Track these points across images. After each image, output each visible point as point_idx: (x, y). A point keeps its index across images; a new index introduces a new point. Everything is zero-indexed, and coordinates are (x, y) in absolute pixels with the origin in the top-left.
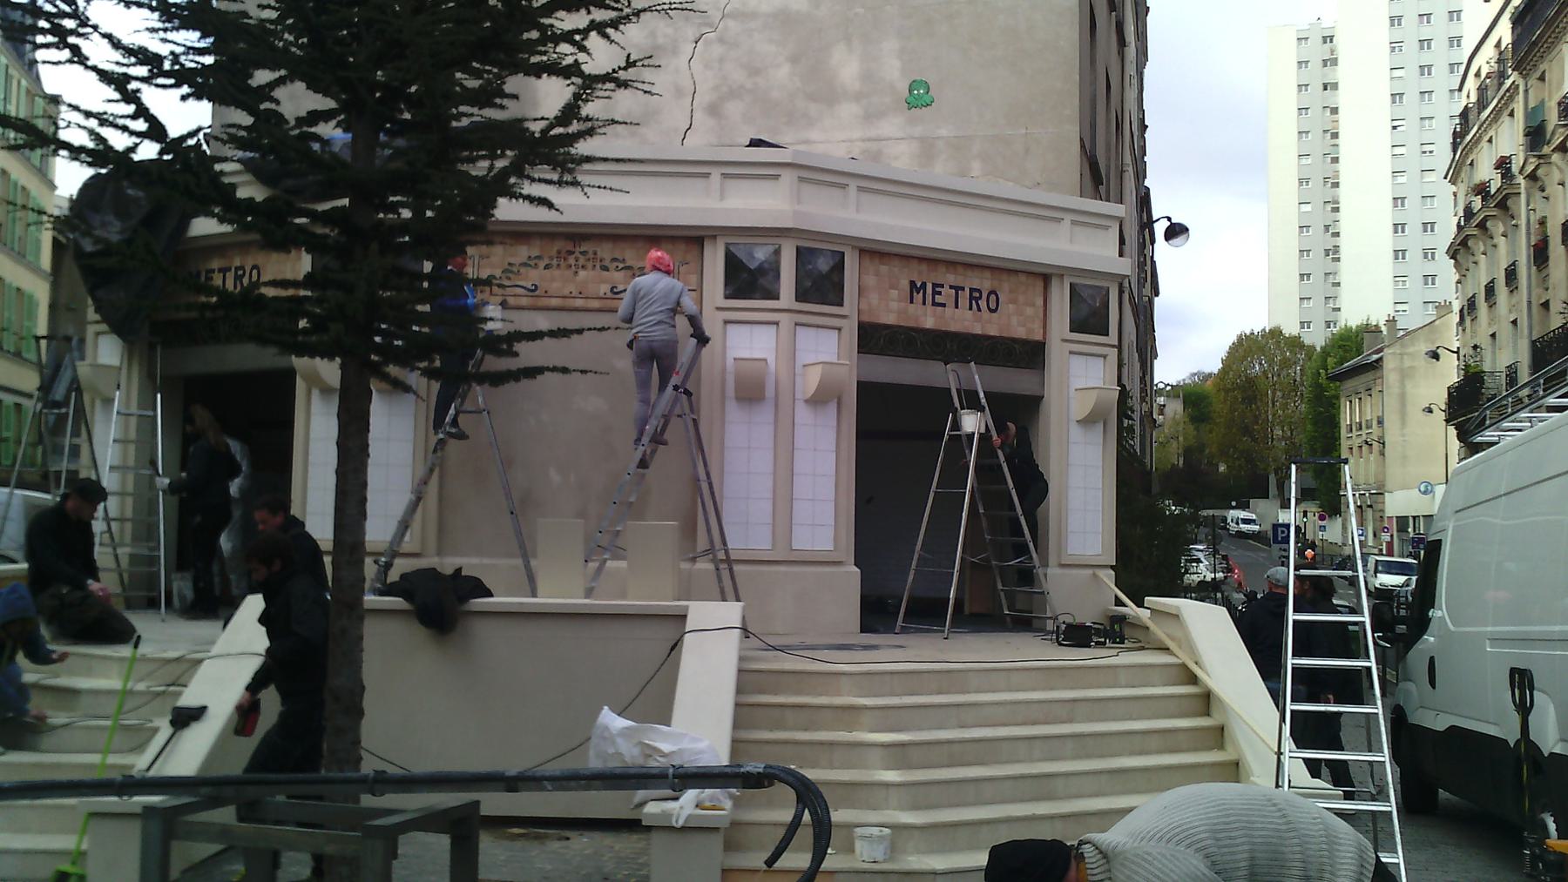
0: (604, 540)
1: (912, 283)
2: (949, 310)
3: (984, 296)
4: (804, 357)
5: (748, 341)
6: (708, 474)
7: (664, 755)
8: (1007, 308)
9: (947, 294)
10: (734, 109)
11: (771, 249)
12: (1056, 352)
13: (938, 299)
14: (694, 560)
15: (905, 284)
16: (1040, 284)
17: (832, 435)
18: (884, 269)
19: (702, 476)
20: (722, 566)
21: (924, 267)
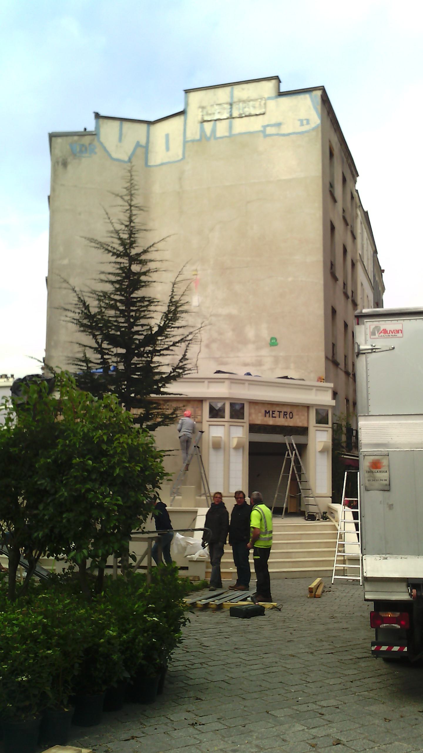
0: (175, 490)
1: (266, 411)
2: (277, 419)
3: (288, 414)
4: (233, 435)
5: (216, 431)
6: (204, 471)
7: (192, 544)
8: (296, 417)
9: (276, 414)
10: (214, 346)
11: (222, 404)
12: (312, 430)
13: (274, 415)
14: (200, 496)
15: (263, 411)
16: (306, 409)
17: (241, 457)
18: (257, 407)
19: (203, 472)
20: (208, 498)
21: (269, 406)
